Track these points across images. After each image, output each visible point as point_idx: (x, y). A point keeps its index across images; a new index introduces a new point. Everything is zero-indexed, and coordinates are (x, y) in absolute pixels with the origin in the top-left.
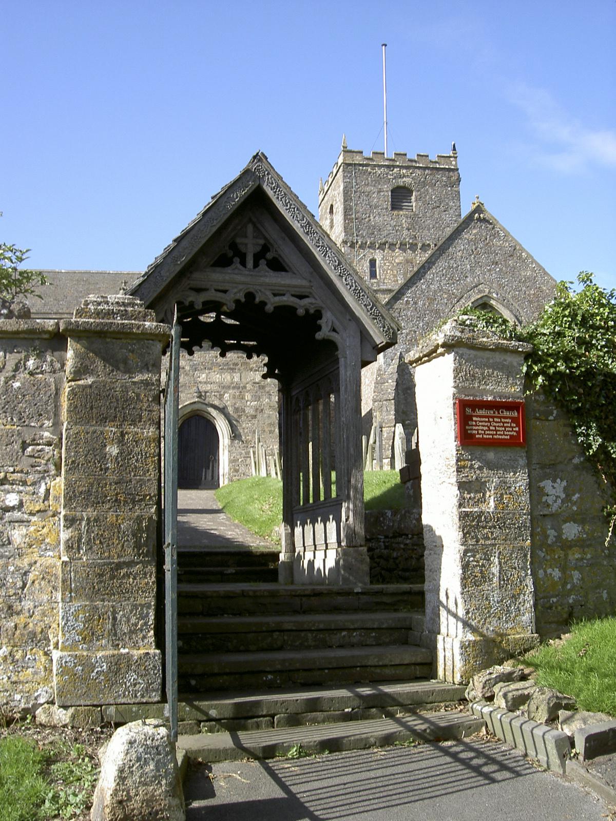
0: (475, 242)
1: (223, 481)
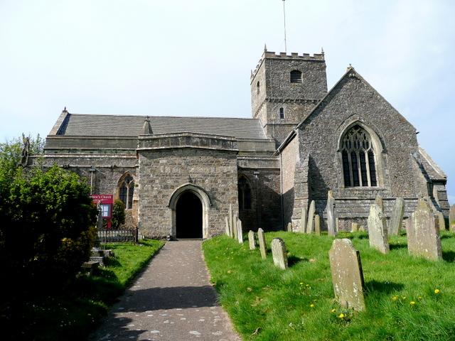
0: (351, 90)
1: (205, 234)
